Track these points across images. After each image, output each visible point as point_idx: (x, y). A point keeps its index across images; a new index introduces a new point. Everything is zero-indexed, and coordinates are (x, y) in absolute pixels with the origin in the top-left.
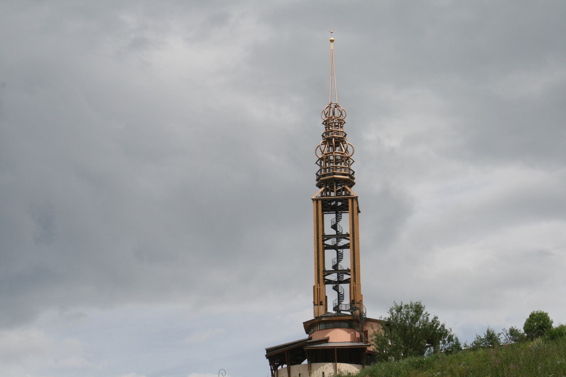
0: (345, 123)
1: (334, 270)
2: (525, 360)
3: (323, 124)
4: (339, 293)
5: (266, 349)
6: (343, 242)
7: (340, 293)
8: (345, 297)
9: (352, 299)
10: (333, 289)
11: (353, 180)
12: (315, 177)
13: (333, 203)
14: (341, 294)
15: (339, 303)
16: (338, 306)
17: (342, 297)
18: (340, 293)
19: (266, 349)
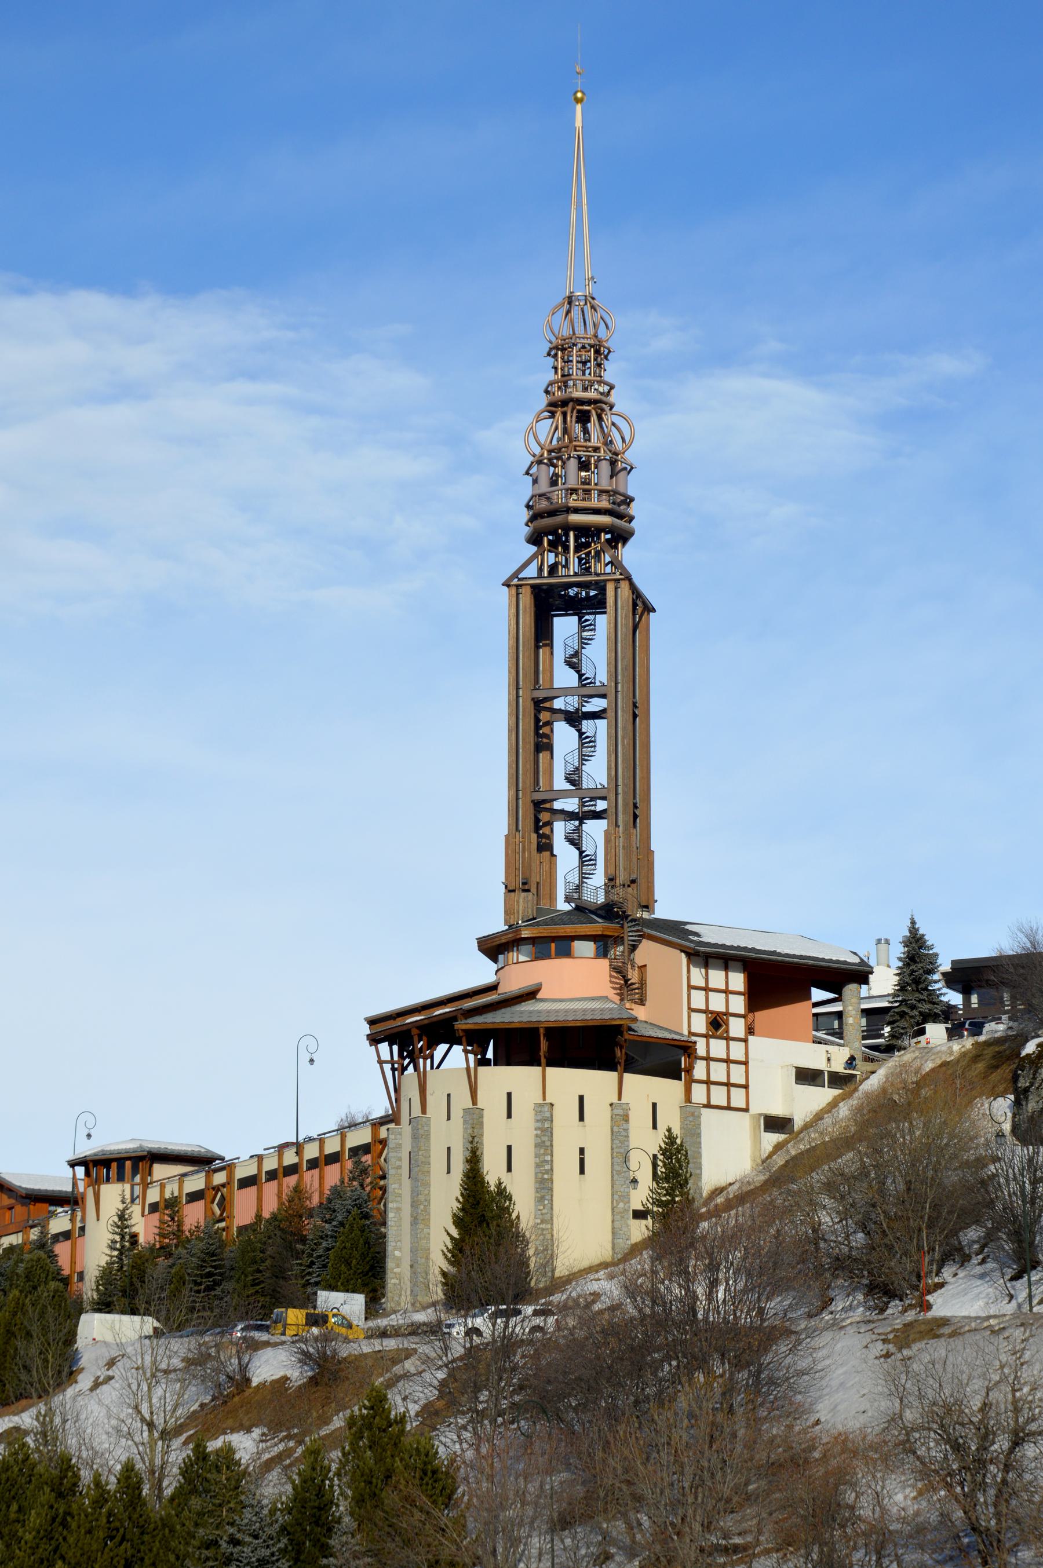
0: (610, 351)
1: (574, 788)
2: (756, 1267)
3: (549, 354)
4: (581, 853)
5: (366, 1019)
6: (596, 705)
7: (585, 733)
8: (597, 628)
9: (611, 871)
10: (566, 661)
11: (630, 522)
12: (525, 515)
13: (572, 592)
14: (587, 737)
15: (583, 876)
16: (578, 770)
17: (591, 744)
18: (585, 733)
19: (366, 1019)
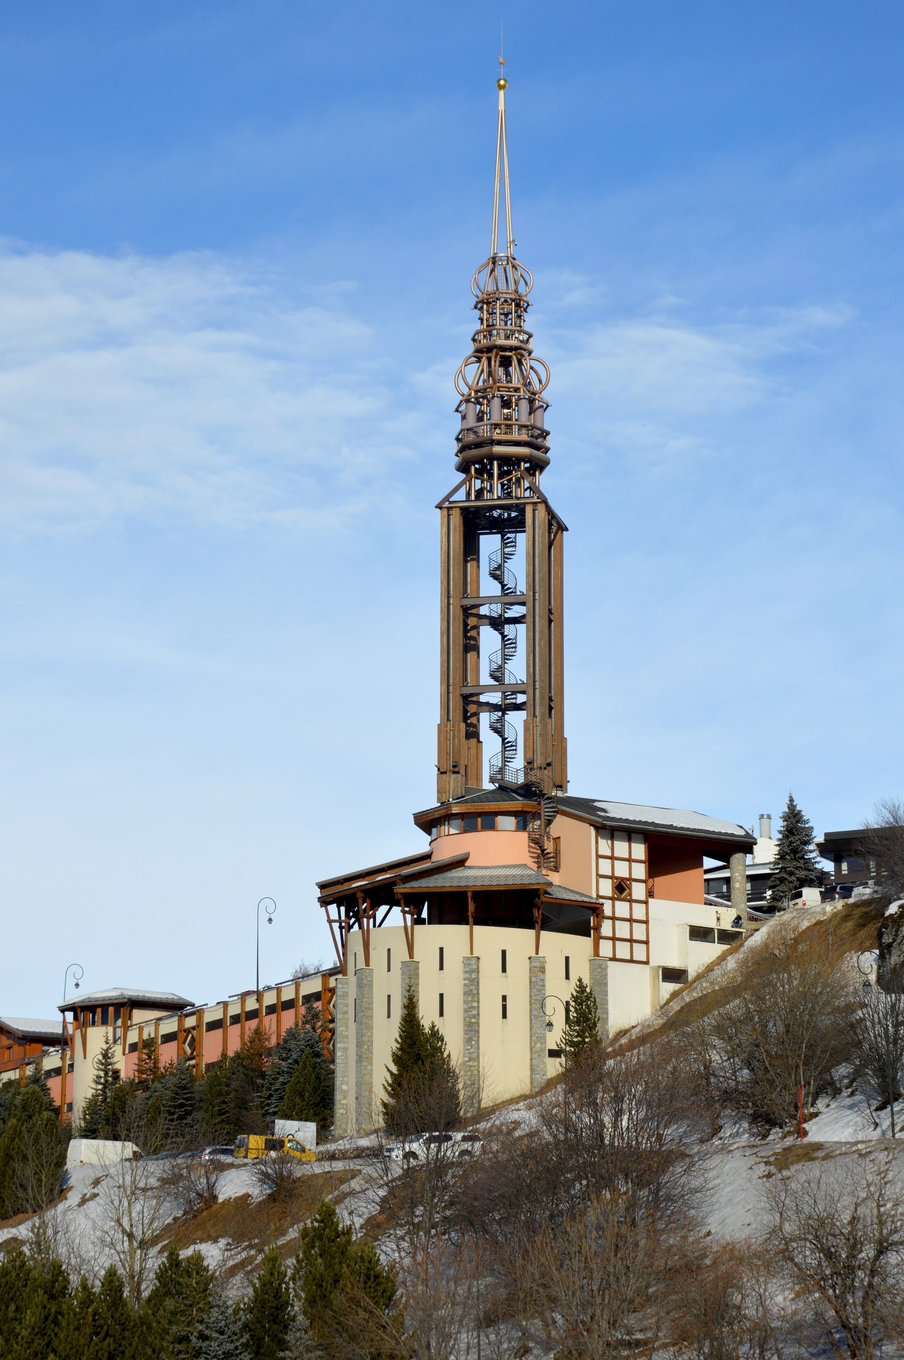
0: (528, 305)
1: (497, 683)
2: (656, 1099)
3: (476, 307)
4: (504, 739)
5: (317, 884)
6: (516, 611)
7: (507, 636)
8: (517, 544)
9: (530, 756)
10: (490, 574)
11: (546, 452)
12: (455, 447)
13: (496, 514)
14: (509, 639)
15: (505, 760)
16: (501, 668)
17: (512, 646)
18: (507, 636)
19: (317, 884)
